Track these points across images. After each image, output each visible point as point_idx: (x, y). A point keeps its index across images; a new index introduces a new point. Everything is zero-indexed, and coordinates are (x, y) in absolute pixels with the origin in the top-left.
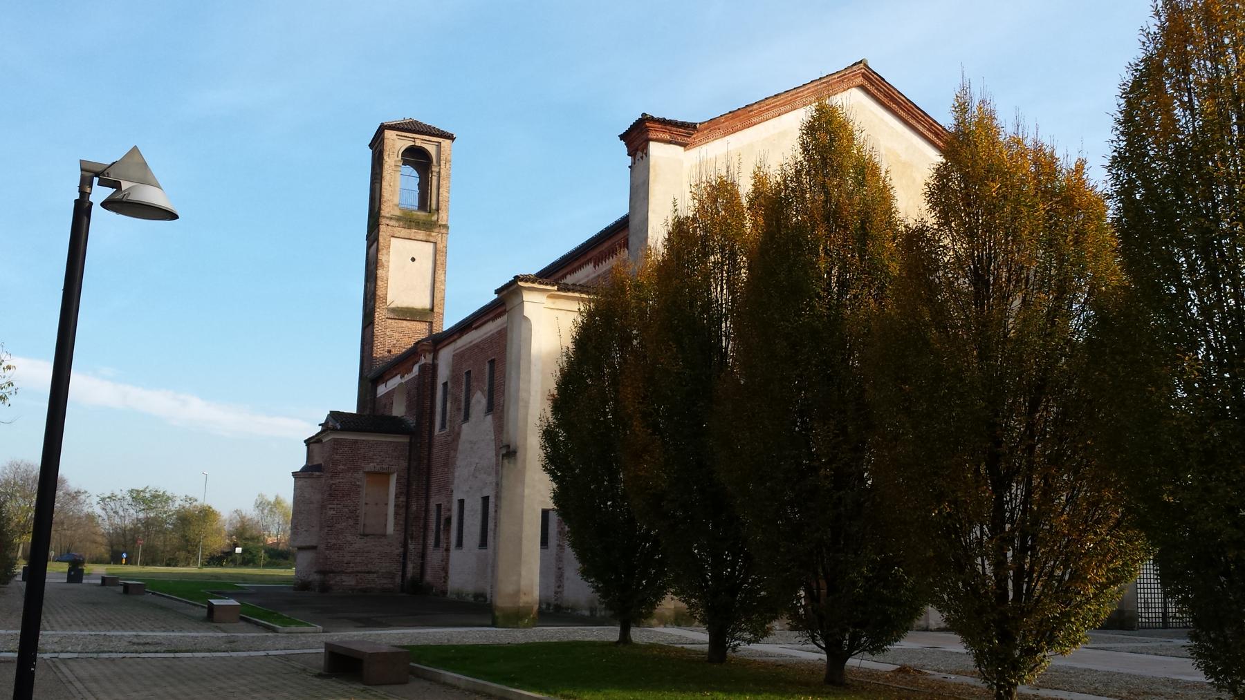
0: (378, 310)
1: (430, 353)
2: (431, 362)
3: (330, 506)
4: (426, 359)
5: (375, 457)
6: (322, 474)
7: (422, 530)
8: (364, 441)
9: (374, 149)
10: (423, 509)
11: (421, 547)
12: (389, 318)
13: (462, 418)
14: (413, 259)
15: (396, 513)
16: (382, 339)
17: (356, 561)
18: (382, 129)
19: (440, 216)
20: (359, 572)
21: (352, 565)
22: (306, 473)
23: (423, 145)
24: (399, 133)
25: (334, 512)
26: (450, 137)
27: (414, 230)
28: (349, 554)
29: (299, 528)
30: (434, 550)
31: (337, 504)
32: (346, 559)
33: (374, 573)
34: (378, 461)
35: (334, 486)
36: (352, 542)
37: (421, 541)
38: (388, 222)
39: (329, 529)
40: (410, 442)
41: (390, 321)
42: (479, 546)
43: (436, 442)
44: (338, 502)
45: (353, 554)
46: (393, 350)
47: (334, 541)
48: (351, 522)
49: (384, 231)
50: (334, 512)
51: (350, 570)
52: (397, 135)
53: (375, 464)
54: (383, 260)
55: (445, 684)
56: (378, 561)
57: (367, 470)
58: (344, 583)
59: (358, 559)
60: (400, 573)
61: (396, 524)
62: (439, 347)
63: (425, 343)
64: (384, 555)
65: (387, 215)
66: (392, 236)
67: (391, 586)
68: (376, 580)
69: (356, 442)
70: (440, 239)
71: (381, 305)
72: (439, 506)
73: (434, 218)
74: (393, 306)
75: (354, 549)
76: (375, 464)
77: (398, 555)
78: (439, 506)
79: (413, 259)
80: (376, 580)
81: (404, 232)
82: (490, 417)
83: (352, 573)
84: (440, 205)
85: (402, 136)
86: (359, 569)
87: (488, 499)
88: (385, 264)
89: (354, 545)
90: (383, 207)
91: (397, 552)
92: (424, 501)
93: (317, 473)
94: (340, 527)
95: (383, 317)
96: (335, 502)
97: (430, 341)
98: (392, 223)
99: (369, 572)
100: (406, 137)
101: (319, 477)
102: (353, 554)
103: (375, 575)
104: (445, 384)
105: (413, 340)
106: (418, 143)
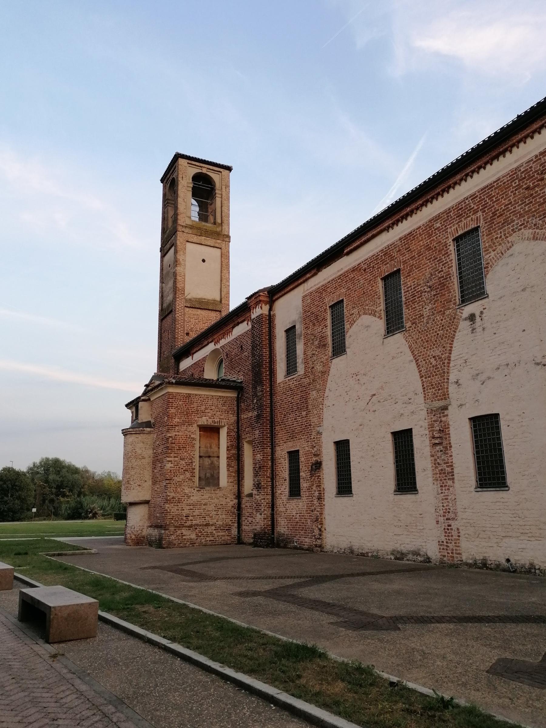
0: (178, 299)
1: (266, 305)
2: (267, 313)
3: (168, 459)
4: (264, 310)
5: (207, 411)
6: (152, 429)
7: (269, 480)
8: (196, 395)
9: (165, 182)
10: (269, 458)
11: (270, 497)
12: (187, 307)
13: (330, 354)
14: (204, 261)
15: (229, 465)
16: (182, 324)
17: (195, 514)
18: (178, 156)
19: (223, 227)
20: (197, 525)
21: (190, 518)
22: (137, 429)
23: (208, 173)
24: (190, 162)
25: (172, 465)
26: (229, 169)
27: (203, 238)
28: (188, 507)
29: (132, 483)
30: (289, 499)
31: (174, 457)
32: (185, 513)
33: (212, 525)
34: (209, 414)
35: (170, 439)
36: (190, 494)
37: (269, 491)
38: (184, 229)
39: (167, 482)
40: (238, 397)
41: (187, 309)
42: (395, 491)
43: (279, 389)
44: (176, 455)
45: (192, 507)
46: (191, 333)
47: (172, 495)
48: (188, 475)
49: (180, 238)
50: (172, 465)
51: (189, 523)
52: (188, 163)
53: (208, 418)
54: (181, 260)
55: (94, 554)
56: (215, 513)
57: (200, 424)
58: (184, 537)
59: (197, 512)
60: (236, 525)
61: (229, 476)
62: (276, 297)
63: (261, 294)
64: (220, 506)
65: (183, 224)
66: (187, 241)
67: (229, 538)
68: (214, 532)
69: (189, 395)
70: (223, 245)
71: (180, 296)
72: (294, 456)
73: (218, 229)
74: (189, 297)
75: (192, 502)
76: (208, 418)
77: (232, 507)
78: (294, 456)
79: (204, 261)
80: (214, 532)
81: (195, 239)
82: (398, 338)
83: (191, 526)
84: (223, 219)
85: (192, 164)
86: (197, 522)
87: (497, 422)
88: (182, 262)
89: (192, 498)
90: (179, 217)
91: (232, 503)
92: (269, 450)
93: (149, 429)
94: (178, 480)
95: (182, 305)
96: (172, 455)
97: (266, 293)
98: (187, 230)
99: (207, 525)
100: (195, 165)
101: (150, 433)
102: (192, 507)
103: (213, 528)
104: (290, 331)
105: (206, 325)
106: (204, 171)
